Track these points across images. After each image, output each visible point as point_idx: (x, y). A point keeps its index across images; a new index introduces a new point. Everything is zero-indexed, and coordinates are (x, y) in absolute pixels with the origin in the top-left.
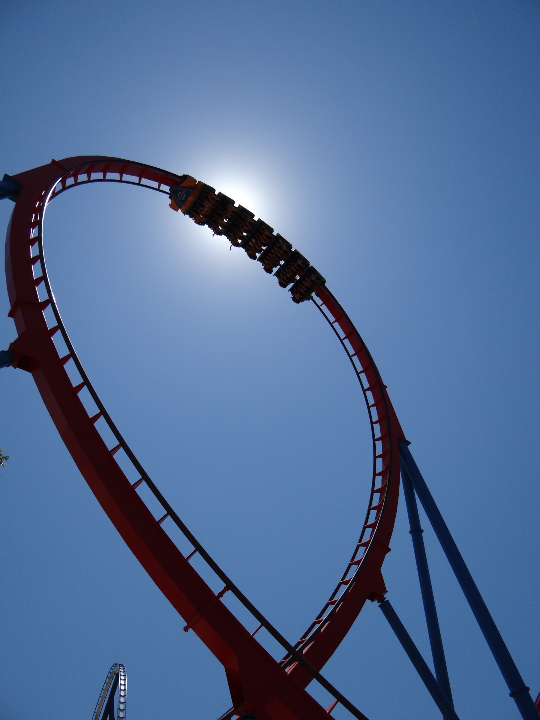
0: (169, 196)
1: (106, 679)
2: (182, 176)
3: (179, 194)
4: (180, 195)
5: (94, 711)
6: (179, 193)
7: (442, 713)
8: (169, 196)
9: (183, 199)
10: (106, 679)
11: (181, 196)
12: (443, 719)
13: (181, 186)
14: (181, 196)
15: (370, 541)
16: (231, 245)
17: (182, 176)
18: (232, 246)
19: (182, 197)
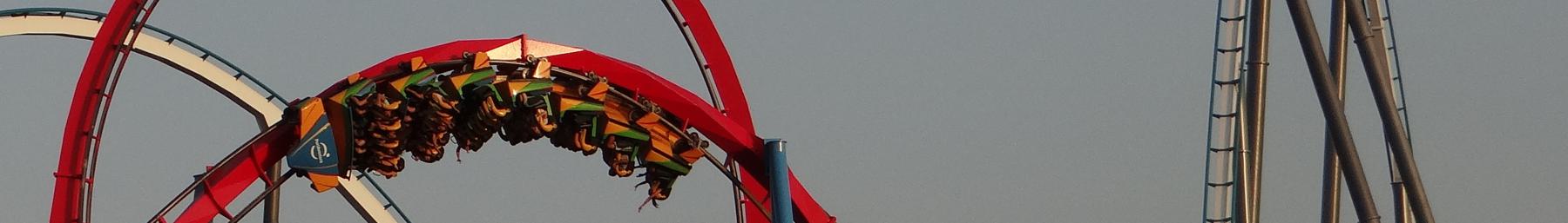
0: (295, 174)
1: (1404, 101)
2: (533, 140)
3: (314, 157)
4: (317, 155)
5: (1403, 80)
6: (310, 152)
7: (1326, 118)
8: (295, 174)
9: (328, 155)
10: (1404, 101)
11: (319, 152)
12: (1394, 221)
13: (302, 137)
14: (319, 152)
15: (205, 174)
16: (289, 101)
17: (533, 140)
18: (285, 102)
19: (322, 154)
